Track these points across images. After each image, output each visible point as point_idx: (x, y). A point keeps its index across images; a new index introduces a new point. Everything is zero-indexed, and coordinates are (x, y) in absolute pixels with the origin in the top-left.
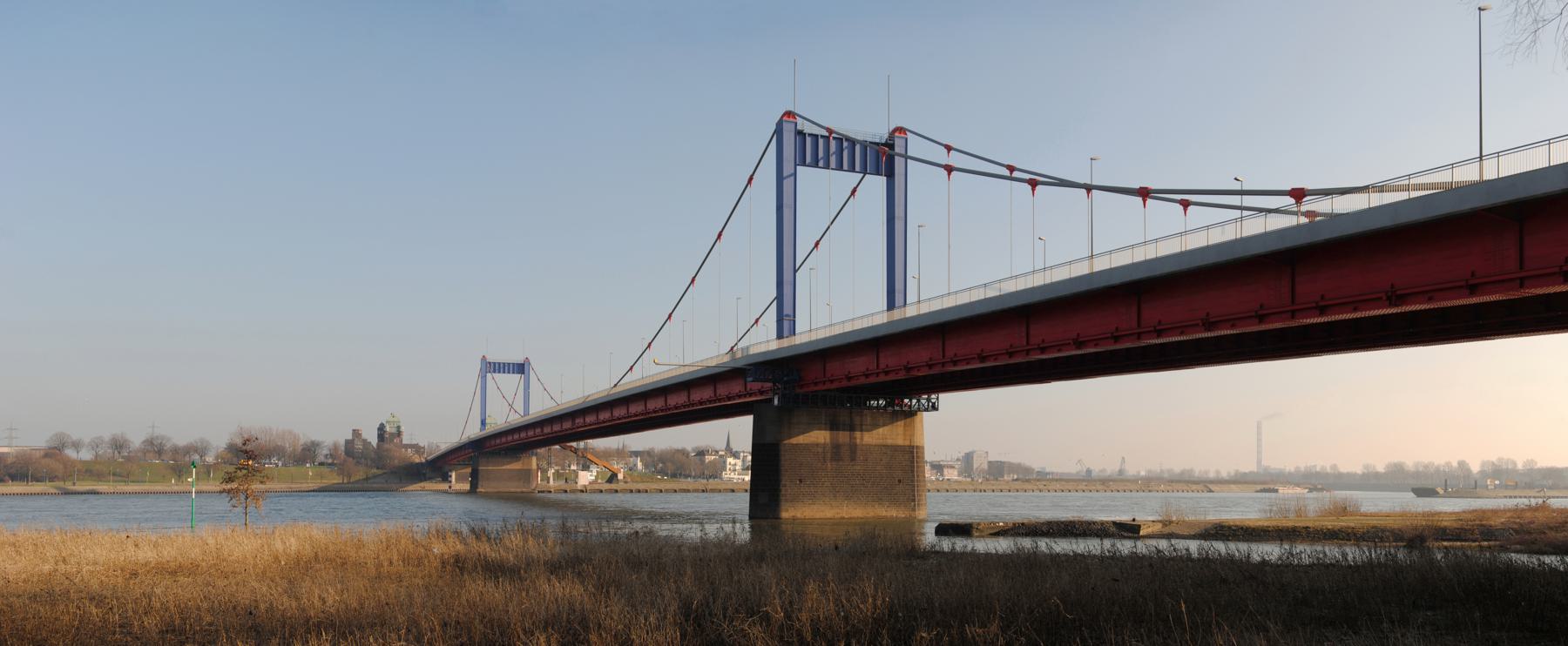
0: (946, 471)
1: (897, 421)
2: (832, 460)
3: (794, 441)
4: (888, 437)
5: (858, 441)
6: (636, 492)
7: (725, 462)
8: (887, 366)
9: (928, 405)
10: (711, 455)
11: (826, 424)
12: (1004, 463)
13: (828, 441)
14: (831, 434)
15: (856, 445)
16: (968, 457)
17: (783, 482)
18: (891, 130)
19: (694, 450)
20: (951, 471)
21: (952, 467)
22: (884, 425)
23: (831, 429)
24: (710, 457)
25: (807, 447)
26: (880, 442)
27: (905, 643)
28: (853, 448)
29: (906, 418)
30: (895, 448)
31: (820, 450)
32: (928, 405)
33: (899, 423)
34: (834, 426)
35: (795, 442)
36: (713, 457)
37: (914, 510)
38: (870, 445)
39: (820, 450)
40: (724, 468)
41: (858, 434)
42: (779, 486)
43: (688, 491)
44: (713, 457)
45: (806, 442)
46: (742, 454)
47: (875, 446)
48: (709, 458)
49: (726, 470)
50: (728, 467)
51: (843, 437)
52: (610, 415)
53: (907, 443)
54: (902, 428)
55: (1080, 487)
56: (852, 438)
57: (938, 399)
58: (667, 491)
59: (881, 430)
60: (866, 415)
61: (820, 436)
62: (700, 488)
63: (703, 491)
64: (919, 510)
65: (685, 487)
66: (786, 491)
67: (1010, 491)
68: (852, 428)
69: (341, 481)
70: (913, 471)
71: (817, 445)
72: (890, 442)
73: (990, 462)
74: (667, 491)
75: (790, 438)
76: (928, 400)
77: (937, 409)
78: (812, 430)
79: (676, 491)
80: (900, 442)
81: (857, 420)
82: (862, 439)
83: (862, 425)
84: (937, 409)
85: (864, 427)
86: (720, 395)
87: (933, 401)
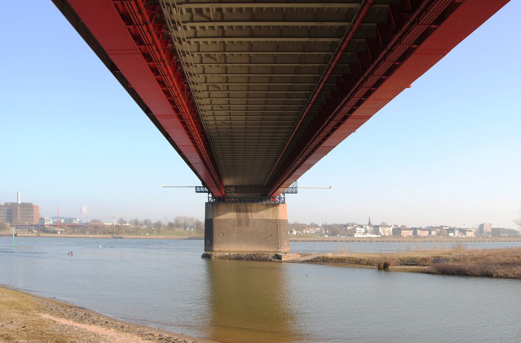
0: (467, 233)
1: (269, 208)
2: (237, 226)
3: (220, 217)
4: (265, 215)
5: (250, 217)
6: (293, 241)
7: (356, 229)
10: (350, 226)
11: (234, 210)
12: (500, 229)
13: (235, 217)
14: (237, 214)
15: (249, 219)
16: (481, 226)
17: (215, 235)
20: (470, 233)
21: (471, 231)
22: (262, 210)
23: (237, 212)
24: (349, 227)
25: (226, 220)
26: (261, 218)
27: (520, 317)
28: (248, 221)
29: (273, 207)
30: (268, 221)
31: (232, 222)
33: (270, 209)
34: (238, 211)
35: (220, 218)
36: (351, 227)
37: (278, 248)
38: (255, 219)
39: (232, 222)
40: (355, 232)
41: (250, 214)
42: (213, 237)
43: (316, 241)
44: (351, 227)
45: (225, 218)
46: (364, 226)
47: (258, 219)
48: (349, 228)
49: (356, 233)
50: (357, 231)
51: (242, 215)
53: (274, 218)
54: (272, 211)
55: (516, 240)
56: (247, 216)
58: (307, 241)
59: (261, 212)
60: (254, 206)
61: (231, 215)
62: (321, 240)
63: (322, 241)
64: (281, 248)
65: (315, 240)
66: (216, 239)
67: (475, 242)
68: (247, 211)
69: (198, 236)
70: (277, 231)
71: (230, 219)
72: (265, 218)
73: (492, 229)
74: (307, 241)
75: (217, 216)
78: (228, 213)
79: (310, 241)
80: (271, 218)
81: (249, 208)
82: (252, 216)
83: (251, 210)
85: (252, 211)
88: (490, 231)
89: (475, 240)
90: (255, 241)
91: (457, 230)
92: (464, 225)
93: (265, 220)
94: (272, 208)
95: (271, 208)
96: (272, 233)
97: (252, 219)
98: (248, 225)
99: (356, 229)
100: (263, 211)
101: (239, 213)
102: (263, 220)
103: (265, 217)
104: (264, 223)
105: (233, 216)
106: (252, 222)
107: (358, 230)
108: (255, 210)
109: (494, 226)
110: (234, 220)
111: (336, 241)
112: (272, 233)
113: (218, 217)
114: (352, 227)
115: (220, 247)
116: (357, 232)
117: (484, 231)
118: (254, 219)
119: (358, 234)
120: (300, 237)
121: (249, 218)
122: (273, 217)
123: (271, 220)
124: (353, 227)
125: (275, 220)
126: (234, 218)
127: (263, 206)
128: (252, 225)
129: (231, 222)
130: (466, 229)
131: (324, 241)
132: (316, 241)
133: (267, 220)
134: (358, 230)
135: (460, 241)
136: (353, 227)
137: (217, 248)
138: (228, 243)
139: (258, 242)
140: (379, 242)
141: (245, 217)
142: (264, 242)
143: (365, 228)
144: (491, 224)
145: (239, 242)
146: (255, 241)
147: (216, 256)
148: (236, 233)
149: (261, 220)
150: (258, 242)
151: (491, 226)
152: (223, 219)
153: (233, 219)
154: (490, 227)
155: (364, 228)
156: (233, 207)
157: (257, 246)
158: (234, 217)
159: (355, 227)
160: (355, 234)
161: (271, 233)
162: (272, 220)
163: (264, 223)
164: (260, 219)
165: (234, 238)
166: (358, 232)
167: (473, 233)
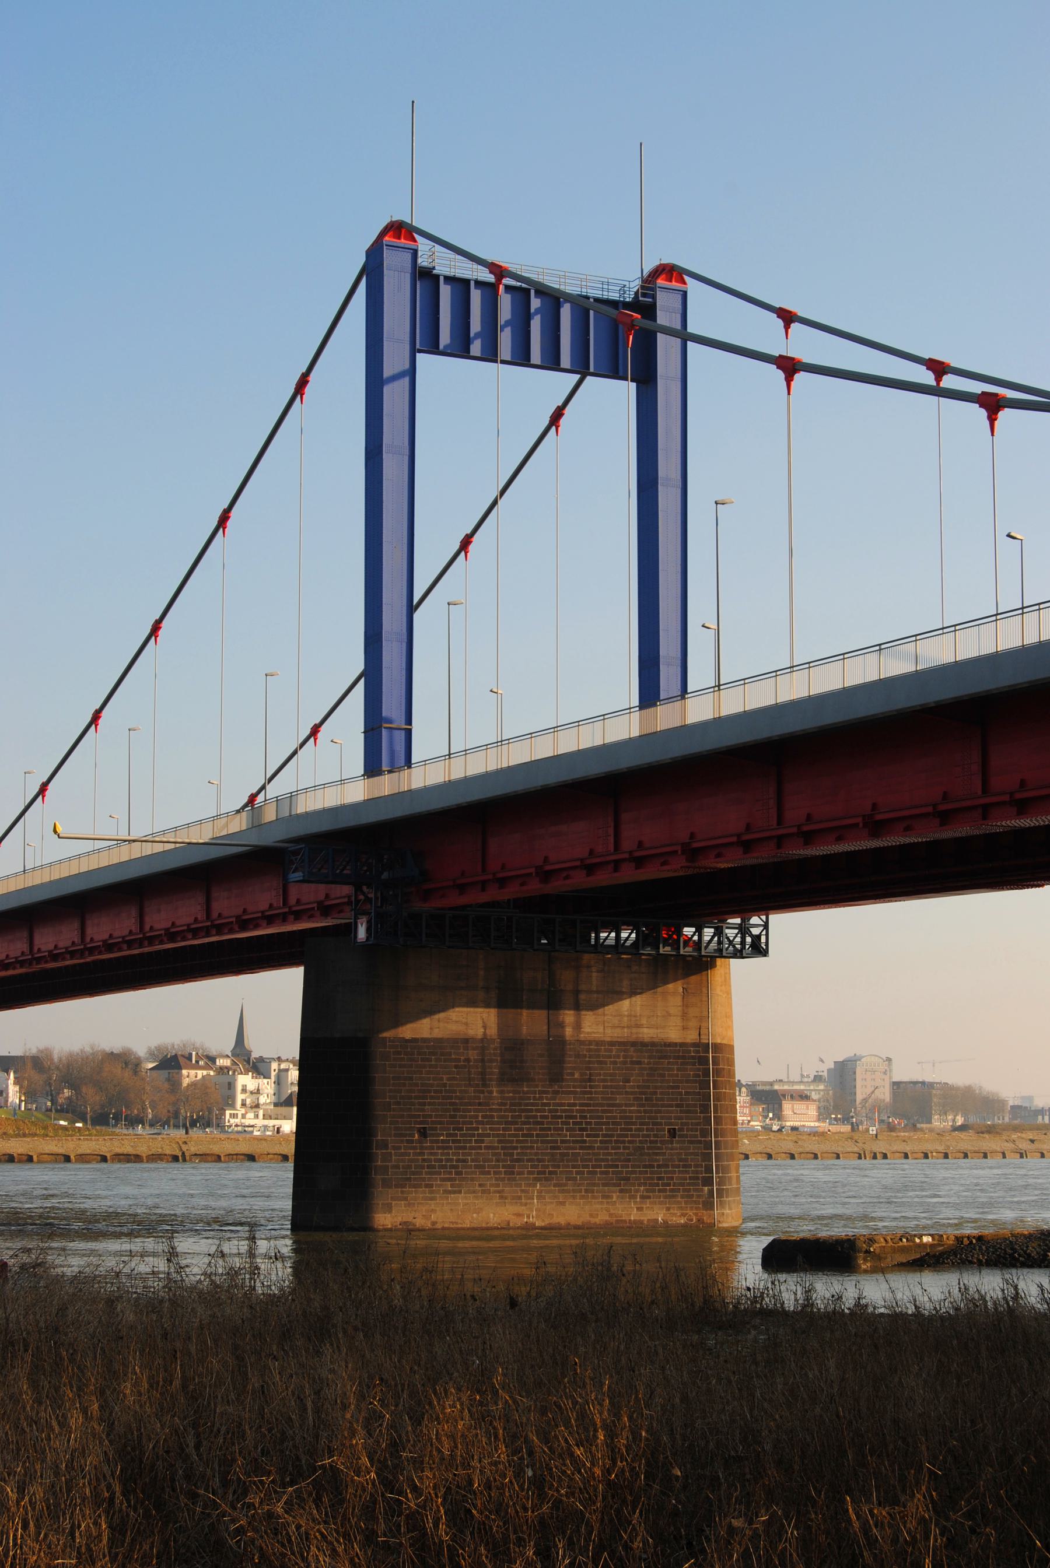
0: (787, 1107)
1: (666, 982)
2: (505, 1079)
3: (407, 1031)
5: (569, 1031)
8: (640, 844)
9: (743, 942)
10: (197, 1066)
12: (931, 1085)
13: (493, 1031)
18: (646, 273)
19: (152, 1055)
20: (800, 1106)
21: (804, 1097)
24: (192, 1072)
25: (437, 1047)
30: (661, 1050)
31: (473, 1055)
32: (743, 942)
33: (670, 986)
36: (201, 1073)
37: (709, 1205)
39: (473, 1055)
40: (229, 1101)
41: (568, 1017)
43: (137, 1158)
45: (437, 1034)
46: (274, 1066)
47: (612, 1043)
48: (190, 1076)
50: (240, 1097)
52: (25, 947)
53: (691, 1037)
57: (766, 926)
58: (83, 1158)
59: (625, 1004)
60: (589, 967)
62: (168, 1152)
63: (175, 1159)
65: (128, 1149)
68: (553, 1002)
70: (706, 1109)
71: (466, 1041)
72: (647, 1033)
73: (896, 1085)
74: (83, 1158)
76: (744, 930)
77: (764, 953)
80: (673, 1034)
81: (566, 978)
82: (578, 1026)
83: (577, 992)
84: (764, 953)
86: (39, 950)
87: (755, 931)
88: (888, 1099)
89: (941, 1148)
90: (594, 1166)
91: (744, 1090)
92: (822, 1061)
93: (644, 1044)
94: (680, 982)
95: (675, 980)
96: (681, 1118)
97: (581, 1043)
98: (556, 1077)
99: (231, 1086)
100: (634, 999)
101: (510, 1013)
102: (634, 1044)
103: (645, 1030)
104: (639, 1063)
105: (480, 1023)
106: (578, 1056)
107: (244, 1090)
108: (597, 992)
109: (903, 1073)
110: (484, 1043)
111: (251, 1158)
112: (681, 1118)
113: (400, 1029)
114: (205, 1072)
115: (409, 1205)
116: (239, 1103)
117: (859, 1097)
118: (590, 1043)
119: (243, 1111)
120: (35, 1135)
121: (563, 1036)
122: (684, 1028)
123: (676, 1044)
124: (212, 1073)
125: (695, 1045)
126: (485, 1034)
127: (635, 968)
128: (576, 1076)
129: (468, 1060)
130: (771, 1084)
131: (184, 1160)
132: (137, 1158)
133: (653, 1044)
134: (244, 1090)
135: (878, 1155)
136: (212, 1073)
137: (390, 1212)
138: (449, 1180)
139: (607, 1173)
140: (113, 1160)
141: (546, 1027)
142: (640, 1172)
143: (278, 1076)
144: (889, 1060)
145: (513, 1173)
146: (594, 1166)
147: (877, 1251)
148: (493, 1123)
149: (623, 1044)
150: (607, 1173)
151: (891, 1071)
152: (424, 1040)
153: (482, 1040)
154: (887, 1078)
155: (273, 1074)
156: (482, 973)
157: (603, 1197)
158: (485, 1027)
159: (221, 1068)
160: (228, 1112)
161: (676, 1118)
162: (682, 1045)
163: (639, 1063)
164: (621, 1044)
165: (487, 1148)
166: (244, 1104)
167: (812, 1110)
